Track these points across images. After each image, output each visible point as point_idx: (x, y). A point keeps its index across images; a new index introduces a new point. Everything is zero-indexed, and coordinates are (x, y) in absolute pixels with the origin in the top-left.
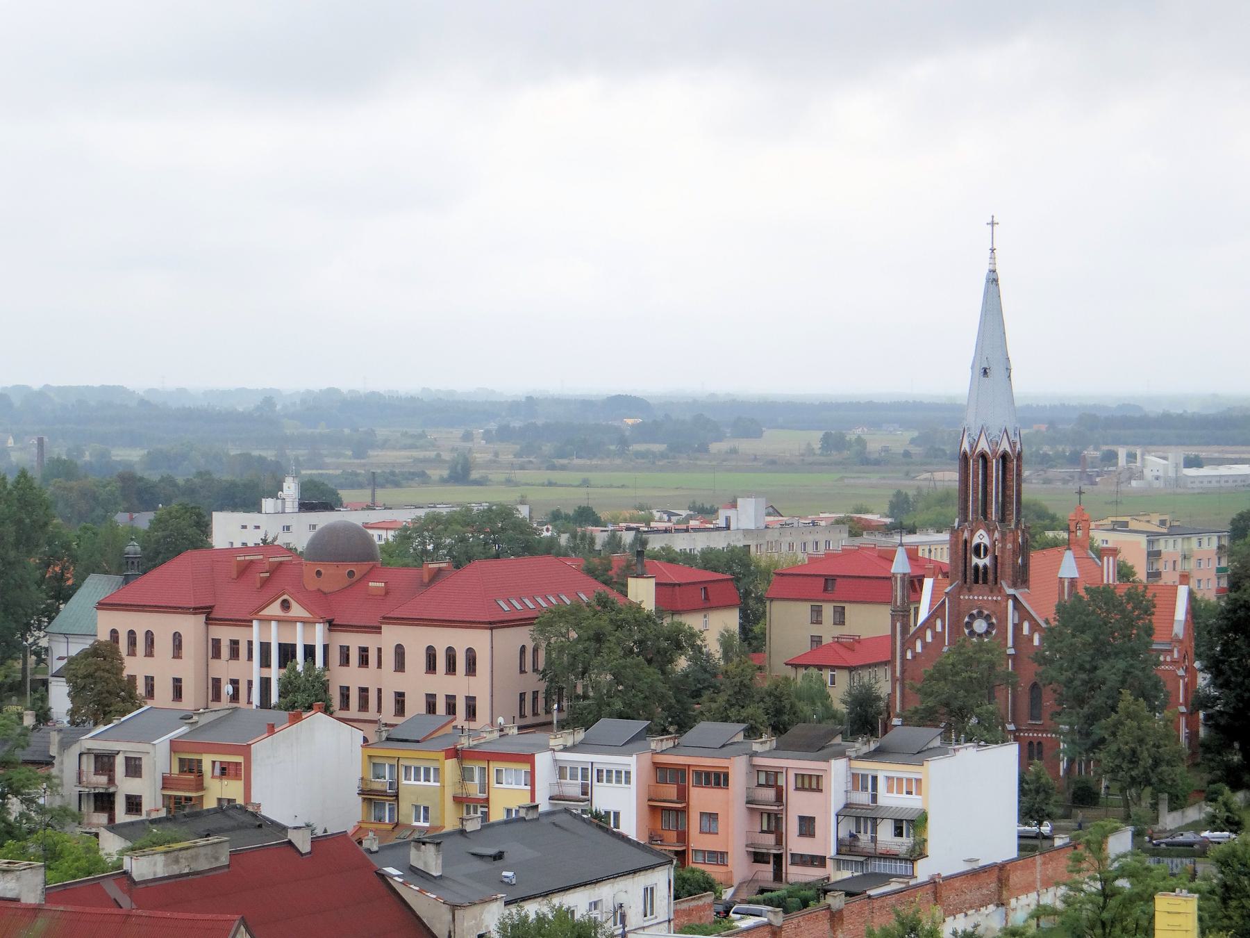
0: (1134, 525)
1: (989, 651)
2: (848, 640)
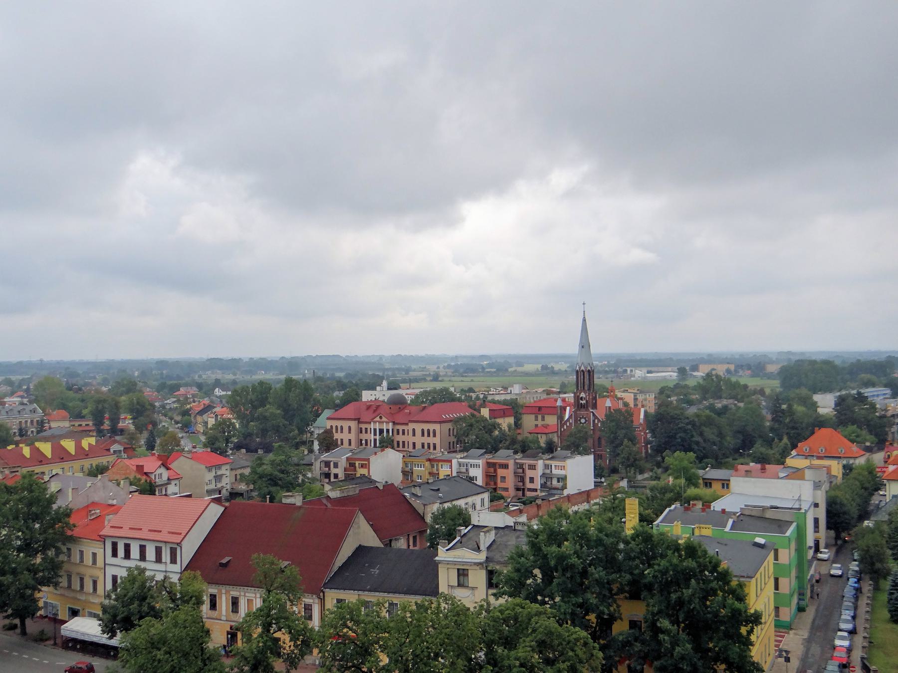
1: (585, 428)
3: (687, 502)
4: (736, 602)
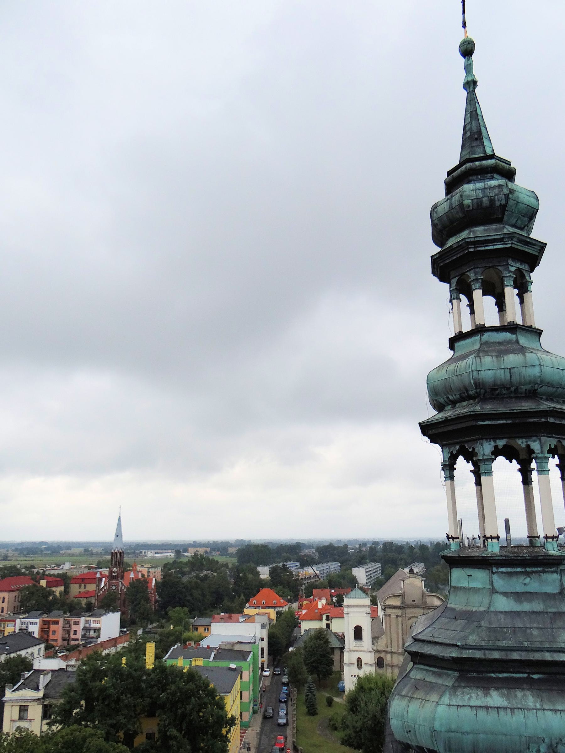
3: (184, 642)
4: (220, 711)
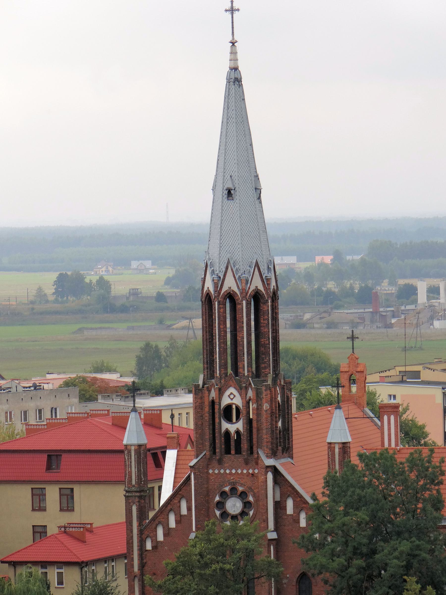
0: (426, 375)
1: (243, 536)
2: (77, 530)
